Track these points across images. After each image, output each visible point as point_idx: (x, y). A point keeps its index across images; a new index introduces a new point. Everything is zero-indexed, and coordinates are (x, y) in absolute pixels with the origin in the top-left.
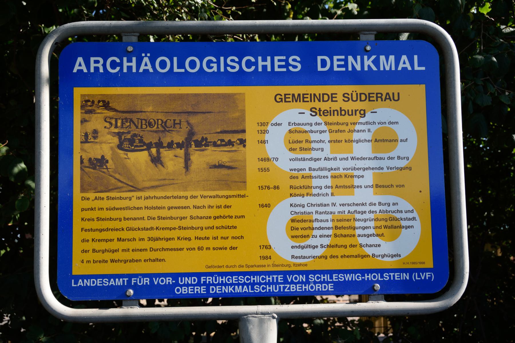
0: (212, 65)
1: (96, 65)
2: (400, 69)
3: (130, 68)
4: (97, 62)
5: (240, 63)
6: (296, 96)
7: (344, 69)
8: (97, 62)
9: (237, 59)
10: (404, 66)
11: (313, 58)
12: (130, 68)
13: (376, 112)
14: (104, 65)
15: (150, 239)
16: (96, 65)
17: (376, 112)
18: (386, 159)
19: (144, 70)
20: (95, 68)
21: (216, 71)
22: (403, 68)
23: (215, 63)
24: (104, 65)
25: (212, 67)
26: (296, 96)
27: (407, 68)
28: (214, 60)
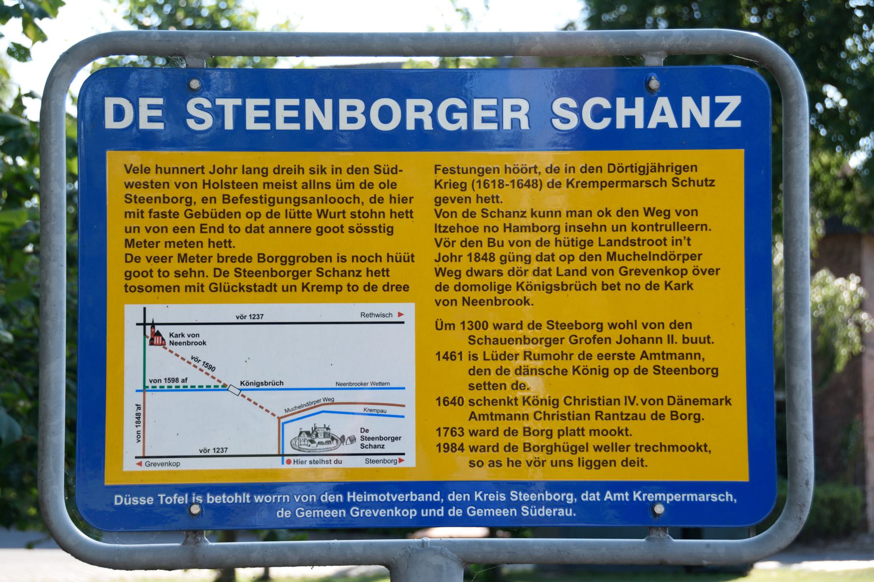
0: (456, 116)
1: (516, 115)
2: (652, 125)
3: (630, 120)
4: (419, 109)
5: (578, 111)
6: (323, 216)
7: (296, 126)
8: (419, 109)
9: (573, 104)
10: (663, 119)
11: (831, 109)
12: (630, 120)
13: (403, 323)
14: (434, 115)
15: (600, 356)
16: (516, 115)
17: (403, 323)
18: (648, 417)
19: (659, 124)
20: (513, 121)
21: (465, 127)
22: (659, 124)
23: (462, 111)
24: (434, 115)
25: (456, 121)
26: (323, 216)
27: (667, 124)
28: (461, 104)
